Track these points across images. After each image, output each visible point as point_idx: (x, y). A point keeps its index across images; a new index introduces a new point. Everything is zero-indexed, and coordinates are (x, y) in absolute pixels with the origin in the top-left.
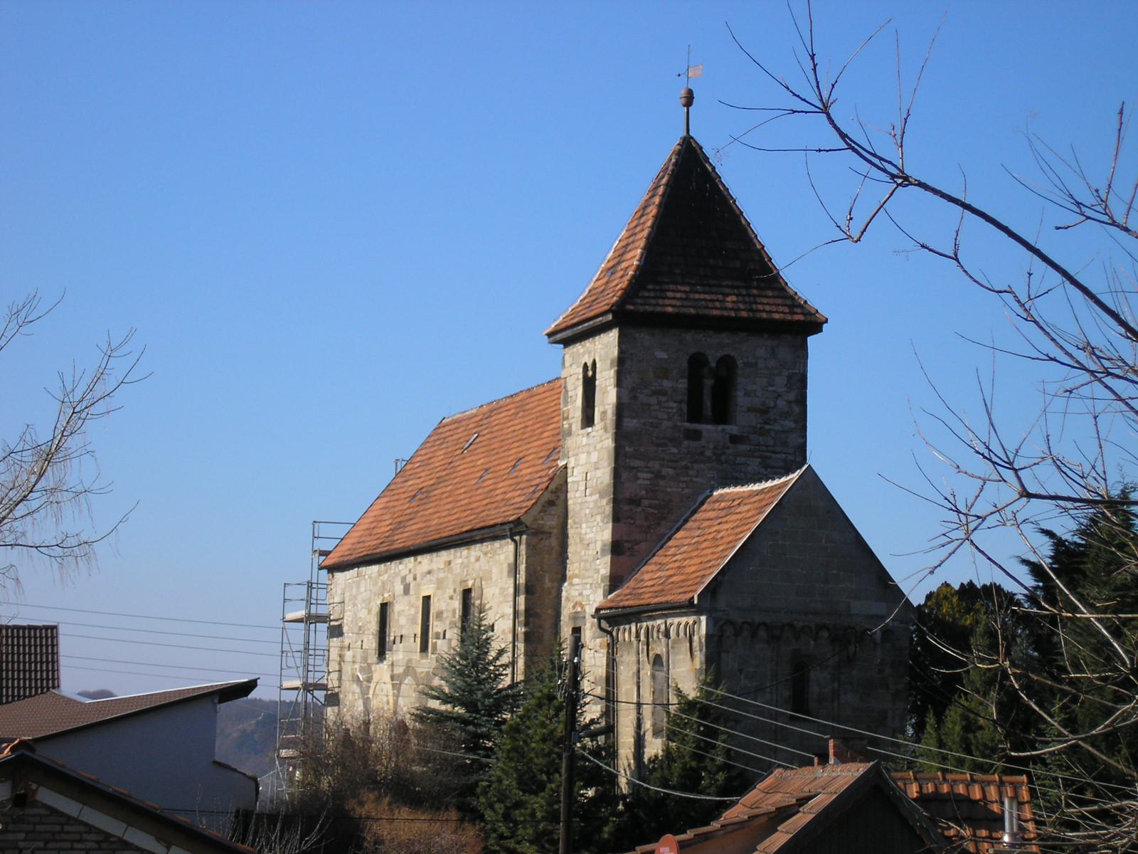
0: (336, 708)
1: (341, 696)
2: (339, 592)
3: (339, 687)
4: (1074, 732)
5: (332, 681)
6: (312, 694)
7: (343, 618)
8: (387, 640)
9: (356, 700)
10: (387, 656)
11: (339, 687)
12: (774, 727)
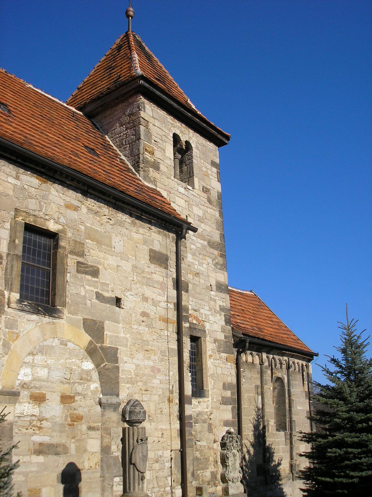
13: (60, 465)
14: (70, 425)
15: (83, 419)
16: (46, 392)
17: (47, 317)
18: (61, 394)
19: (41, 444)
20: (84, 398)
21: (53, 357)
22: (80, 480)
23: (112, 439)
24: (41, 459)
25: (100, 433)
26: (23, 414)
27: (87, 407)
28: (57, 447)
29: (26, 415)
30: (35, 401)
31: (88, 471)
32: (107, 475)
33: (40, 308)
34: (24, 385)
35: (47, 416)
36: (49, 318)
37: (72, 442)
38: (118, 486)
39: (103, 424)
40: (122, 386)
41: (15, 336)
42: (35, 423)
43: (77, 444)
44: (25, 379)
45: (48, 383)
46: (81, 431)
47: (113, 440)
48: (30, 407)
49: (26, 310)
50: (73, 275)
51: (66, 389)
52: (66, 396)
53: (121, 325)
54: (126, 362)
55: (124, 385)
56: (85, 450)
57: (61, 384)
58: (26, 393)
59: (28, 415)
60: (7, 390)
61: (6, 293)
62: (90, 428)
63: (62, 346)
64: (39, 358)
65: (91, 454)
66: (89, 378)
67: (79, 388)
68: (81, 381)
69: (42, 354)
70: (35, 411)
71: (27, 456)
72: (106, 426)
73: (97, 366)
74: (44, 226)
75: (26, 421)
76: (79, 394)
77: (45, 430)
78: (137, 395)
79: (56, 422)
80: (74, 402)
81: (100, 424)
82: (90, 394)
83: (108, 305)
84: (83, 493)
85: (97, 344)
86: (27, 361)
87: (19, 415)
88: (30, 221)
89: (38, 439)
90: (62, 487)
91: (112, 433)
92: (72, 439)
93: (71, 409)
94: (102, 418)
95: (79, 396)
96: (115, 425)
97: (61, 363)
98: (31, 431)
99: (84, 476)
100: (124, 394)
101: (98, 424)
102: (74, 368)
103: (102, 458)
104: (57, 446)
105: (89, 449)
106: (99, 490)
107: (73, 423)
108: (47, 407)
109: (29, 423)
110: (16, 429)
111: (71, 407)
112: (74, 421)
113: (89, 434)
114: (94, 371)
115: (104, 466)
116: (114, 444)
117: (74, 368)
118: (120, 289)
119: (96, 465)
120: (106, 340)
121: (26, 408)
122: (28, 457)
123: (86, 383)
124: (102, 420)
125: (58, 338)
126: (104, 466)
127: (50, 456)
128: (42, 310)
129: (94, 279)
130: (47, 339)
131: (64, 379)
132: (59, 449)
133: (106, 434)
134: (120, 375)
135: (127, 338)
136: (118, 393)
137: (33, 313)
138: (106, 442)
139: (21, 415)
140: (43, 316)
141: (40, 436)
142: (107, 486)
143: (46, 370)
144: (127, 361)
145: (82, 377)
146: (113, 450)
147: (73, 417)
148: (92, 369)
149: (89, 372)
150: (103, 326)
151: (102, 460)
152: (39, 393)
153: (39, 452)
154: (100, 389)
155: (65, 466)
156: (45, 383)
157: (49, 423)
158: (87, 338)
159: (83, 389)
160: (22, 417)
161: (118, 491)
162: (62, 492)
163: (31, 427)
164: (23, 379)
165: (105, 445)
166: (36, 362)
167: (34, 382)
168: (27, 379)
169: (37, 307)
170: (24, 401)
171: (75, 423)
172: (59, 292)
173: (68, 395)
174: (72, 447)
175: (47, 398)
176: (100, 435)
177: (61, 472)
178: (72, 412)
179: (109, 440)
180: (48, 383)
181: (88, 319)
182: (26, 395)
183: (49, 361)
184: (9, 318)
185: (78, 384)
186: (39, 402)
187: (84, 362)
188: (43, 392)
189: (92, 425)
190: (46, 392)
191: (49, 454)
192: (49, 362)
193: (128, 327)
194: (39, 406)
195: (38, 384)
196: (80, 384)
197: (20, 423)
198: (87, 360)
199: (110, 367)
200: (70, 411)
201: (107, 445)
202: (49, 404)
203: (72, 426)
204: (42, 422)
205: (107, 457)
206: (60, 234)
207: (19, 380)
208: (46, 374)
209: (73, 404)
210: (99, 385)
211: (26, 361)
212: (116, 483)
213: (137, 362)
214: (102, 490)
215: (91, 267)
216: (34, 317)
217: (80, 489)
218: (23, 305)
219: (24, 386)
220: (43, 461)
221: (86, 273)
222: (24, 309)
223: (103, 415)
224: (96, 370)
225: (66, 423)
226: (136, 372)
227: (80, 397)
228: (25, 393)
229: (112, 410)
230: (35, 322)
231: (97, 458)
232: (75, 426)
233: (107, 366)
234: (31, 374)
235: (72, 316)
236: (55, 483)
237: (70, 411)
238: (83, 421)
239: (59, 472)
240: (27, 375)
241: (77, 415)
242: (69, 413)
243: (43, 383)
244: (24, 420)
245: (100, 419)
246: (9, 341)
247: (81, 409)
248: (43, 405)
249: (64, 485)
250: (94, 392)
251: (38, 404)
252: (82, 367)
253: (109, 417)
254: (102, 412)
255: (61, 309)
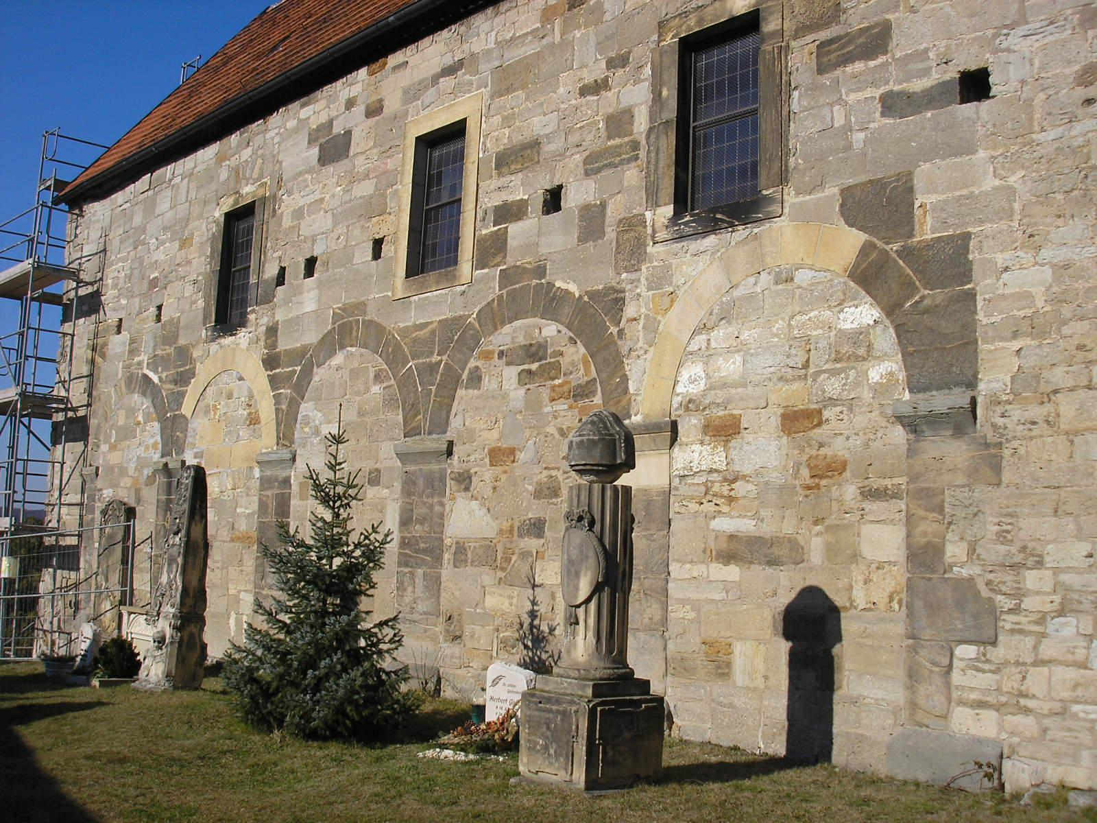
0: (79, 446)
1: (93, 422)
2: (95, 234)
3: (89, 405)
4: (934, 572)
5: (77, 395)
6: (28, 428)
7: (101, 279)
8: (253, 280)
9: (139, 423)
10: (252, 317)
11: (89, 405)
12: (18, 541)
13: (780, 591)
14: (809, 488)
15: (844, 470)
16: (741, 412)
17: (740, 228)
18: (780, 411)
19: (732, 537)
20: (851, 410)
21: (754, 323)
22: (838, 638)
23: (950, 523)
24: (732, 572)
25: (903, 507)
26: (692, 470)
27: (861, 434)
28: (772, 544)
29: (698, 472)
30: (714, 436)
31: (863, 612)
32: (927, 634)
33: (719, 216)
34: (690, 405)
35: (747, 469)
36: (744, 229)
37: (814, 532)
38: (969, 672)
39: (914, 478)
40: (990, 351)
41: (667, 300)
42: (716, 488)
43: (829, 537)
44: (691, 391)
45: (746, 387)
46: (840, 501)
47: (953, 527)
48: (705, 453)
49: (689, 233)
50: (806, 90)
51: (797, 394)
52: (795, 412)
53: (982, 154)
54: (1006, 269)
55: (1001, 344)
56: (855, 557)
57: (780, 384)
58: (694, 421)
59: (701, 471)
60: (654, 421)
61: (648, 215)
62: (871, 494)
63: (780, 287)
64: (720, 336)
65: (874, 566)
66: (862, 351)
67: (833, 387)
68: (838, 366)
69: (729, 323)
70: (717, 459)
71: (699, 565)
72: (927, 485)
73: (890, 311)
74: (718, 17)
75: (698, 484)
76: (832, 402)
77: (741, 502)
78: (1059, 371)
79: (767, 483)
80: (819, 424)
81: (902, 480)
82: (867, 395)
83: (929, 115)
84: (846, 673)
85: (888, 248)
86: (695, 349)
87: (682, 474)
88: (689, 28)
89: (724, 524)
90: (784, 646)
91: (946, 505)
92: (816, 523)
93: (810, 445)
94: (910, 461)
95: (836, 406)
96: (961, 480)
97: (778, 329)
98: (708, 507)
99: (849, 626)
100: (1001, 376)
101: (896, 481)
102: (814, 333)
103: (909, 579)
104: (770, 542)
105: (867, 551)
106: (901, 673)
107: (817, 481)
108: (746, 447)
109: (703, 489)
110: (676, 504)
111: (811, 439)
112: (821, 477)
113: (867, 510)
114: (880, 328)
115: (918, 604)
116: (957, 538)
117: (814, 333)
118: (975, 39)
119: (891, 599)
120: (922, 225)
121: (696, 455)
122: (703, 568)
123: (853, 368)
124: (910, 466)
125: (768, 270)
126: (918, 604)
127: (755, 567)
128: (724, 218)
129: (872, 64)
130: (740, 282)
131: (789, 370)
132: (776, 551)
133: (926, 510)
134: (981, 316)
135: (1013, 187)
136: (975, 376)
137: (705, 234)
138: (925, 533)
139: (686, 473)
140: (730, 229)
141: (732, 517)
142: (929, 666)
143: (738, 358)
144: (1010, 263)
145: (837, 352)
146: (953, 560)
147: (816, 466)
148: (872, 323)
149: (861, 334)
150: (909, 184)
151: (910, 587)
152: (725, 416)
153: (727, 557)
154: (902, 376)
155: (793, 595)
156: (740, 390)
157: (750, 487)
158: (852, 240)
159: (844, 385)
160: (690, 478)
161: (972, 689)
162: (784, 659)
163: (709, 497)
164: (687, 391)
165: (923, 541)
166: (713, 344)
167: (712, 392)
168: (695, 390)
169: (712, 215)
170: (690, 440)
171: (824, 482)
172: (765, 154)
173: (802, 410)
174: (816, 547)
175: (742, 426)
176: (903, 514)
177: (783, 608)
178: (814, 452)
179: (935, 525)
180: (746, 387)
181: (856, 186)
182: (695, 426)
183: (746, 334)
184: (654, 267)
185: (827, 375)
186: (724, 438)
187: (845, 310)
188: (735, 412)
189: (876, 483)
190: (741, 412)
191: (752, 563)
192: (745, 336)
193: (1014, 148)
194: (724, 446)
195: (720, 396)
196: (833, 373)
197: (683, 490)
198: (855, 302)
199: (938, 300)
200: (807, 450)
201: (929, 544)
202: (750, 438)
203: (815, 491)
204: (733, 486)
205: (930, 579)
206: (764, 6)
207: (678, 395)
208: (739, 366)
209: (817, 431)
210: (901, 363)
211: (691, 350)
212: (962, 664)
213: (1062, 255)
214: (910, 676)
215: (860, 36)
216: (712, 240)
217: (836, 659)
218: (680, 225)
219: (688, 407)
220: (737, 579)
221: (847, 60)
222: (684, 234)
223: (911, 452)
224: (887, 322)
225: (797, 483)
226: (1055, 289)
227: (839, 409)
228: (689, 426)
229: (950, 432)
230: (709, 253)
231: (896, 578)
232: (823, 490)
233: (926, 302)
234: (703, 376)
235: (808, 197)
236: (768, 632)
237: (807, 450)
238: (847, 474)
239: (778, 610)
240: (696, 380)
241: (828, 460)
242: (805, 457)
243: (733, 391)
244: (693, 484)
245: (904, 467)
246: (655, 316)
247: (839, 441)
248: (733, 443)
249: (790, 644)
250: (880, 390)
251: (723, 443)
252: (839, 326)
253: (938, 455)
254: (909, 444)
255: (774, 192)
